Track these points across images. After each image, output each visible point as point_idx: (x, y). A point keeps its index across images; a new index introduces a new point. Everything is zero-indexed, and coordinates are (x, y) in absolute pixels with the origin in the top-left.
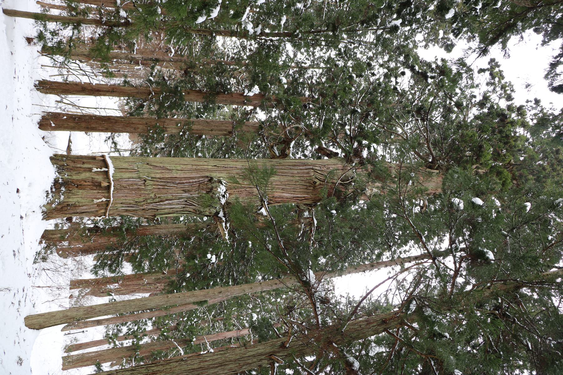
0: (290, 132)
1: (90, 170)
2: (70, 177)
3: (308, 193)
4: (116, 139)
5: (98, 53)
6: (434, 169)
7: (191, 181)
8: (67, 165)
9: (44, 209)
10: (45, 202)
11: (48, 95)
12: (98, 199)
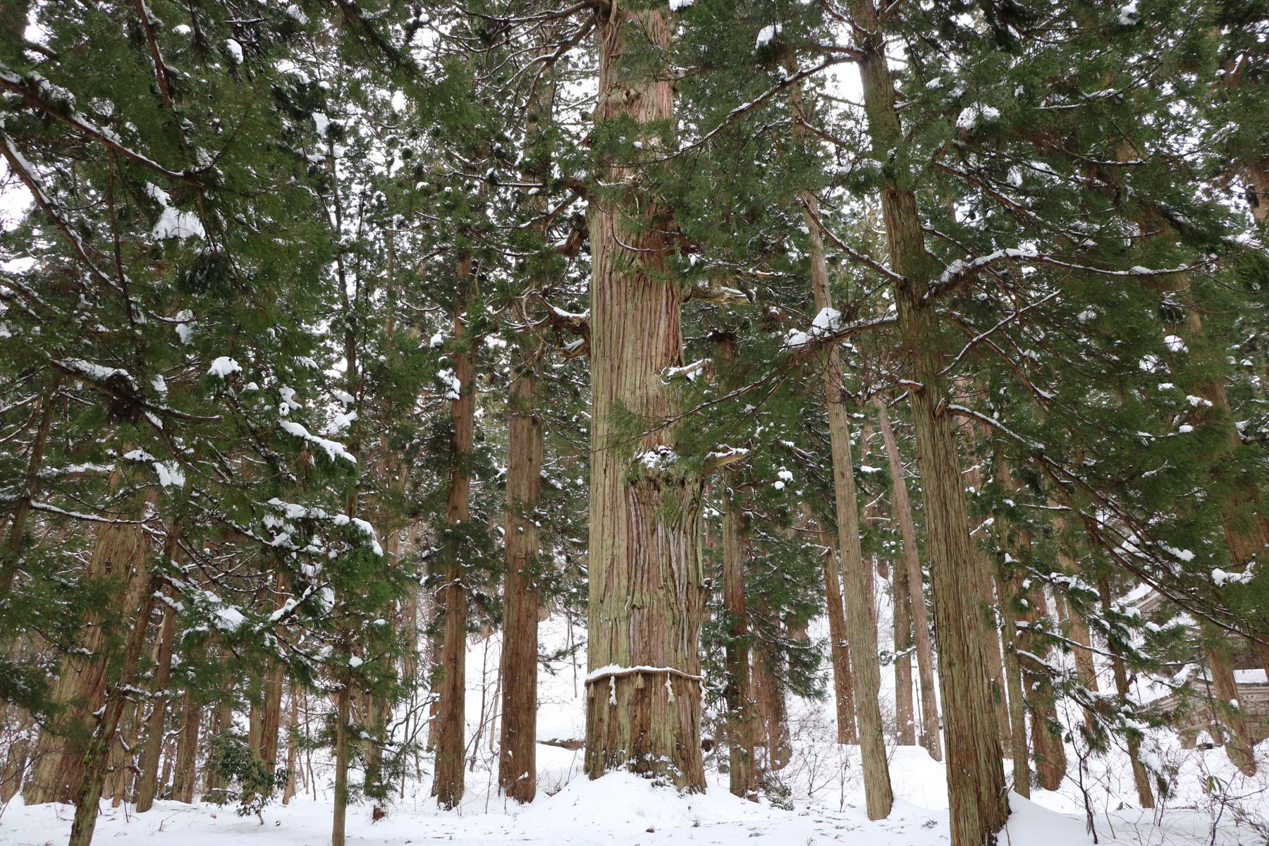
0: (538, 316)
1: (613, 708)
2: (627, 745)
3: (658, 289)
4: (550, 651)
5: (372, 688)
6: (611, 5)
7: (634, 519)
9: (684, 790)
10: (673, 788)
11: (466, 785)
12: (667, 695)
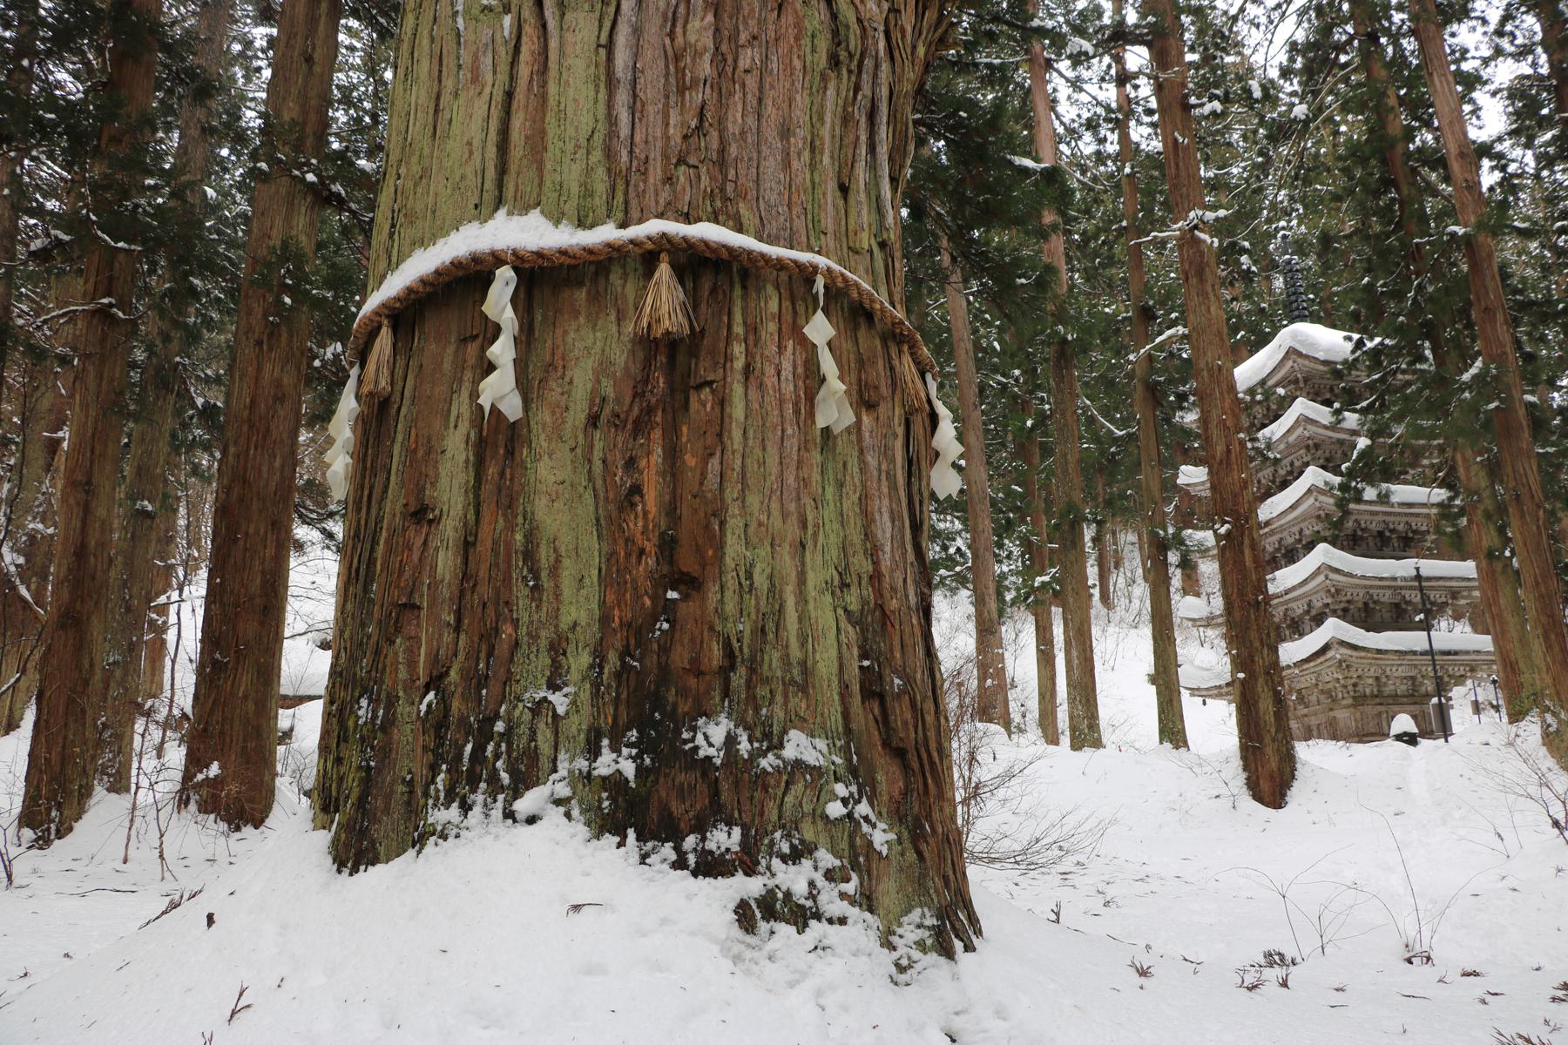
1: (499, 441)
2: (579, 661)
8: (436, 682)
10: (860, 930)
12: (813, 378)
